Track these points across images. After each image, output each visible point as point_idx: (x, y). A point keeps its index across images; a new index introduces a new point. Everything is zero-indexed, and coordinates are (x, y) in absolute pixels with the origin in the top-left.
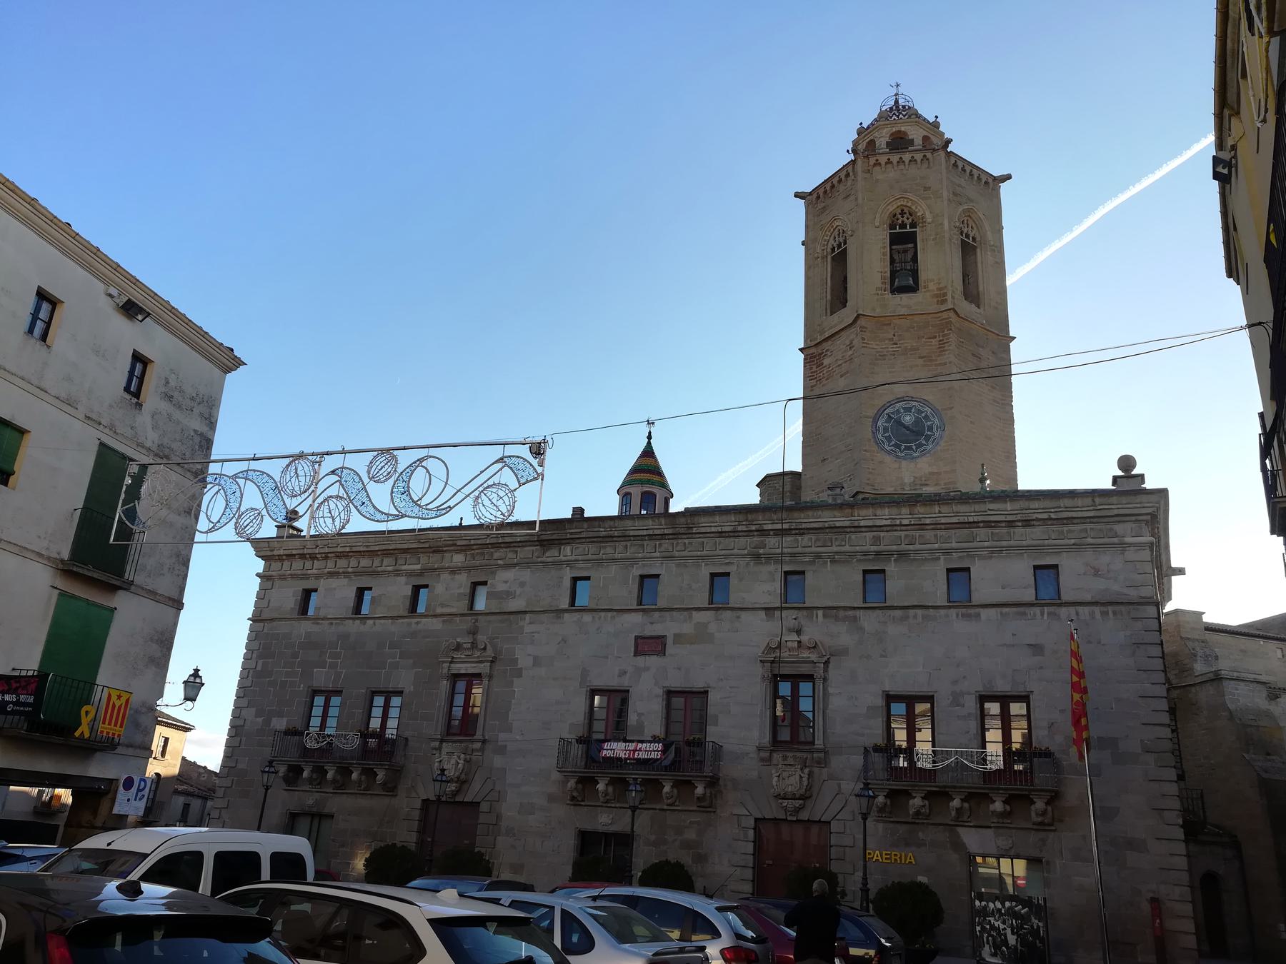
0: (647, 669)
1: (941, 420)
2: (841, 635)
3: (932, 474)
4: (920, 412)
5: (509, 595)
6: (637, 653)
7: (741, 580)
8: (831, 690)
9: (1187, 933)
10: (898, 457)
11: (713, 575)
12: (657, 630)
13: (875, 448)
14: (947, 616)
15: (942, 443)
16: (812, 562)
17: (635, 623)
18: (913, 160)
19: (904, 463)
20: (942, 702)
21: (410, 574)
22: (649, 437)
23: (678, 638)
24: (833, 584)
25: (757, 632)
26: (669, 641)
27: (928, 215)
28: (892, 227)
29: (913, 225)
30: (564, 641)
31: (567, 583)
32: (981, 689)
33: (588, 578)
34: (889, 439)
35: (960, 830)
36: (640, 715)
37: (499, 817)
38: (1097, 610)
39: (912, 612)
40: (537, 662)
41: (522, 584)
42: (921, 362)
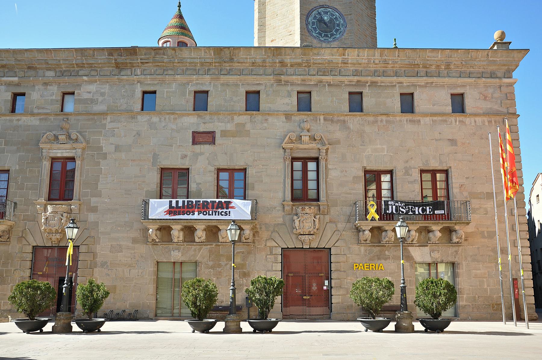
0: (201, 154)
1: (344, 21)
5: (93, 101)
6: (194, 143)
7: (268, 95)
8: (330, 167)
9: (530, 296)
11: (144, 93)
13: (308, 34)
14: (401, 121)
15: (345, 35)
16: (316, 85)
17: (194, 122)
20: (399, 175)
21: (9, 84)
22: (179, 6)
23: (225, 134)
24: (330, 99)
25: (278, 126)
26: (218, 136)
30: (138, 134)
31: (140, 95)
32: (421, 165)
33: (73, 93)
34: (315, 29)
35: (410, 248)
36: (198, 184)
37: (95, 255)
38: (486, 119)
39: (379, 118)
40: (118, 148)
41: (103, 94)
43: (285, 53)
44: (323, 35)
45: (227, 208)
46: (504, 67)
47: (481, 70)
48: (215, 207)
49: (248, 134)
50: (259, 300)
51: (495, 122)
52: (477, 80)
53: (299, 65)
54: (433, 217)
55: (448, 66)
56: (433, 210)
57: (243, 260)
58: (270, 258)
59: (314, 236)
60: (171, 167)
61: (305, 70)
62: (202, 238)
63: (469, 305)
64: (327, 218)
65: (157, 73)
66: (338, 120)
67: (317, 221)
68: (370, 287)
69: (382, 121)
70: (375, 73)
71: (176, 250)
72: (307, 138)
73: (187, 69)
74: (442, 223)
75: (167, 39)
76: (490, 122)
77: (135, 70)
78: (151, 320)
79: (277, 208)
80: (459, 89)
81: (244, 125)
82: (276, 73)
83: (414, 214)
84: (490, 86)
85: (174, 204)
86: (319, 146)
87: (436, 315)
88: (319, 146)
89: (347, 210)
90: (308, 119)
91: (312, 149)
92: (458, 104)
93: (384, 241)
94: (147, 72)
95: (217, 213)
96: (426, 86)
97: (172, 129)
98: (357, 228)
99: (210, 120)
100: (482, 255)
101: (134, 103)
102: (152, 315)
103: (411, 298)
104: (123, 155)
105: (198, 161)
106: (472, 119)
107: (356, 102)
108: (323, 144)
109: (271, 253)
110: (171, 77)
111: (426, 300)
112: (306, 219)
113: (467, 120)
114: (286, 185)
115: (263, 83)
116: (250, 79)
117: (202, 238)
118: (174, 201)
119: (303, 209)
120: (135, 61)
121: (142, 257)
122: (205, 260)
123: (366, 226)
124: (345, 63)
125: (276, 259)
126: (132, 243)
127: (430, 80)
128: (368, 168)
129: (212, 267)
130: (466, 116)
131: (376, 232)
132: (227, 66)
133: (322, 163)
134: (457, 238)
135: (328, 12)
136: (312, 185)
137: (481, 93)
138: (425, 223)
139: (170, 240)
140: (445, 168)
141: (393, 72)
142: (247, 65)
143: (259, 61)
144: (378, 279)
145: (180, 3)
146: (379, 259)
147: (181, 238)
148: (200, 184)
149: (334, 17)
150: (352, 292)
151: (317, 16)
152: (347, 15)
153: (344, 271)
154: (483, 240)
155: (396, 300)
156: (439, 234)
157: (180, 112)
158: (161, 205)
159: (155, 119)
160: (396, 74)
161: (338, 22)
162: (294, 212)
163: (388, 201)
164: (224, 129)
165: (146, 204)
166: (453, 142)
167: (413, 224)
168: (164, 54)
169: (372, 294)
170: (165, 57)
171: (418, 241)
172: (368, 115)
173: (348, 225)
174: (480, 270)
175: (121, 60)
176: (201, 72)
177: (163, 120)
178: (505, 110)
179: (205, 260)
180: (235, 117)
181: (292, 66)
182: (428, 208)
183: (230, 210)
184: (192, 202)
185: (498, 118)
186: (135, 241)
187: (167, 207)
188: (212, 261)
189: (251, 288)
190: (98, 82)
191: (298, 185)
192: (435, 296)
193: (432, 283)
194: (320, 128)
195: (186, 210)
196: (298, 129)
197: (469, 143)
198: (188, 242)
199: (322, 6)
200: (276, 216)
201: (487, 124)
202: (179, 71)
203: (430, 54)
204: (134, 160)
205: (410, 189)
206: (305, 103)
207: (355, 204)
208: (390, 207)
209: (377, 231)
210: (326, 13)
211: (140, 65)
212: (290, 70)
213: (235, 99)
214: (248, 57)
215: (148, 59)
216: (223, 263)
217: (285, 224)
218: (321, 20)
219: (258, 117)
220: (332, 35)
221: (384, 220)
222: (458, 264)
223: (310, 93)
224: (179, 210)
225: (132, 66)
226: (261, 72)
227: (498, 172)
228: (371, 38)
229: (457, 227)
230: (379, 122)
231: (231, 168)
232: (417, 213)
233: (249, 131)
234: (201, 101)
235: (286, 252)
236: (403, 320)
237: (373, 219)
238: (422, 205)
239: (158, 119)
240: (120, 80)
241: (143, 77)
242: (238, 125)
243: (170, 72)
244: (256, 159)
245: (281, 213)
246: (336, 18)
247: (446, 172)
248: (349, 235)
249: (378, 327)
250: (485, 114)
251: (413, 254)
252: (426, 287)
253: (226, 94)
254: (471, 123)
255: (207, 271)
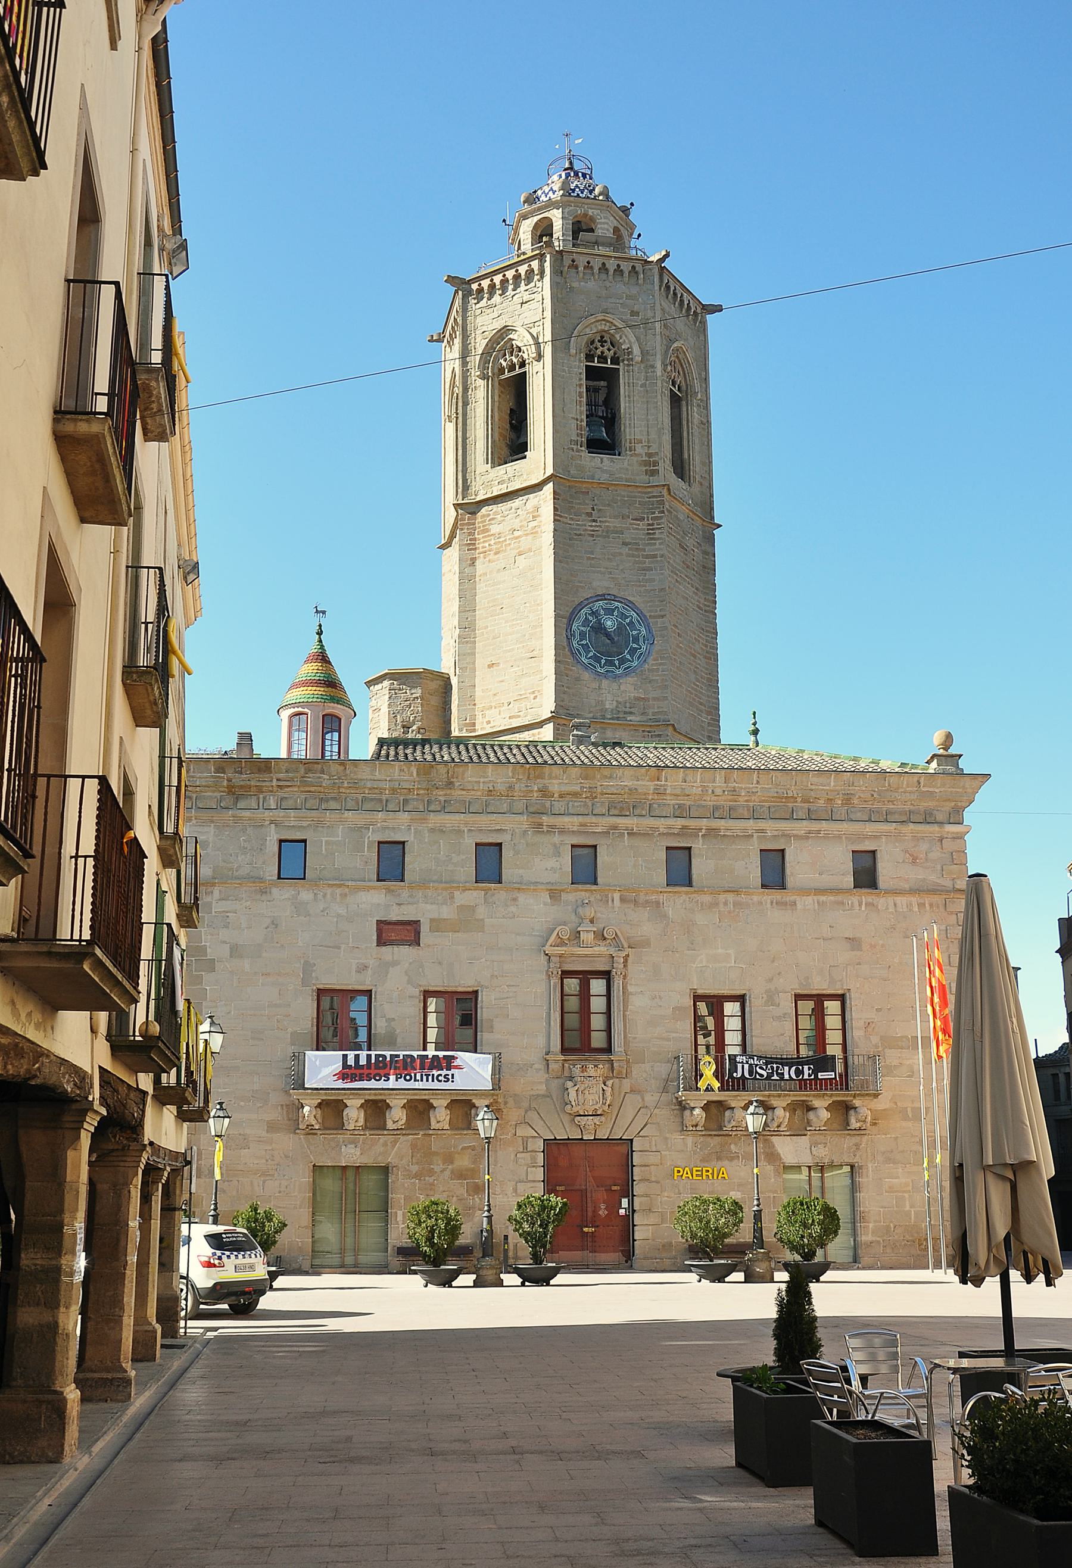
0: (395, 963)
2: (645, 926)
3: (639, 699)
4: (623, 616)
6: (381, 942)
7: (517, 853)
8: (630, 989)
10: (598, 674)
11: (281, 841)
12: (407, 913)
13: (570, 660)
15: (650, 661)
17: (378, 902)
18: (619, 270)
19: (605, 683)
20: (755, 1004)
22: (320, 633)
23: (437, 925)
25: (534, 913)
26: (424, 929)
27: (636, 350)
28: (589, 357)
29: (615, 360)
30: (275, 924)
32: (797, 986)
35: (774, 1139)
38: (914, 900)
39: (722, 897)
40: (236, 951)
42: (625, 550)
43: (550, 774)
44: (603, 661)
45: (449, 1069)
46: (948, 803)
47: (907, 807)
48: (427, 1066)
49: (480, 926)
50: (529, 1233)
51: (931, 905)
52: (899, 826)
53: (575, 794)
54: (816, 1084)
55: (848, 800)
56: (815, 1072)
57: (474, 1162)
58: (524, 1158)
59: (603, 1118)
60: (338, 987)
61: (586, 805)
62: (401, 1123)
63: (879, 1242)
64: (627, 1084)
65: (308, 806)
66: (647, 902)
67: (608, 1090)
68: (706, 1211)
69: (726, 904)
70: (715, 812)
71: (350, 1143)
72: (591, 936)
73: (364, 799)
74: (831, 1096)
75: (300, 709)
76: (921, 905)
77: (264, 798)
78: (307, 1273)
79: (536, 1066)
80: (867, 843)
81: (472, 909)
82: (531, 810)
83: (782, 1079)
84: (923, 838)
85: (351, 1061)
86: (612, 951)
87: (809, 1255)
88: (612, 951)
89: (663, 1069)
90: (592, 899)
91: (600, 956)
92: (866, 875)
93: (729, 1127)
94: (290, 803)
95: (430, 1078)
96: (808, 838)
97: (339, 916)
98: (680, 1103)
99: (410, 900)
100: (903, 1152)
101: (264, 863)
102: (306, 1266)
103: (770, 1228)
104: (246, 965)
105: (389, 976)
106: (890, 900)
107: (680, 869)
108: (620, 948)
109: (525, 1150)
110: (335, 816)
111: (793, 1232)
112: (590, 1088)
113: (882, 902)
114: (552, 1023)
115: (509, 828)
116: (484, 820)
117: (401, 1123)
118: (351, 1055)
119: (584, 1069)
120: (267, 784)
121: (286, 1157)
122: (404, 1161)
123: (697, 1101)
124: (660, 792)
125: (534, 1159)
126: (268, 1132)
127: (815, 826)
128: (700, 992)
129: (417, 1176)
130: (878, 895)
131: (714, 1110)
132: (440, 795)
133: (617, 983)
134: (858, 1121)
135: (613, 610)
136: (597, 1022)
137: (906, 852)
138: (800, 1095)
139: (340, 1126)
140: (840, 992)
141: (748, 810)
142: (479, 793)
143: (501, 787)
144: (718, 1200)
145: (320, 626)
146: (719, 1159)
147: (361, 1122)
148: (393, 1019)
149: (628, 621)
150: (678, 1219)
151: (590, 618)
152: (654, 617)
153: (658, 1182)
154: (904, 1124)
155: (745, 1234)
156: (825, 1115)
157: (354, 883)
158: (327, 1063)
159: (306, 895)
160: (754, 815)
161: (634, 632)
162: (566, 1074)
163: (735, 1056)
164: (435, 916)
165: (298, 1059)
166: (854, 942)
167: (779, 1096)
168: (322, 772)
169: (708, 1222)
170: (325, 776)
171: (790, 1127)
172: (700, 891)
173: (665, 1098)
174: (897, 1177)
175: (238, 780)
176: (391, 807)
177: (320, 896)
178: (948, 884)
179: (404, 1161)
180: (457, 893)
181: (561, 796)
182: (806, 1067)
183: (453, 1071)
184: (384, 1057)
185: (938, 899)
186: (272, 1127)
187: (338, 1066)
188: (417, 1163)
189: (515, 1213)
190: (194, 821)
191: (573, 1021)
192: (805, 1226)
193: (802, 1204)
194: (614, 915)
195: (373, 1071)
196: (573, 917)
197: (883, 945)
198: (373, 1129)
199: (602, 597)
200: (533, 1081)
201: (916, 909)
202: (351, 804)
203: (815, 780)
204: (269, 974)
205: (777, 1032)
206: (585, 868)
207: (677, 1058)
208: (740, 1066)
209: (716, 1109)
210: (610, 612)
211: (275, 789)
212: (559, 807)
213: (455, 859)
214: (482, 780)
215: (292, 779)
216: (437, 1169)
217: (550, 1097)
218: (599, 629)
219: (500, 894)
220: (623, 661)
221: (728, 1090)
222: (861, 1167)
223: (595, 847)
224: (361, 1071)
225: (260, 789)
226: (505, 807)
227: (924, 1012)
228: (705, 657)
229: (857, 1102)
230: (721, 905)
231: (449, 989)
232: (786, 1077)
233: (482, 920)
234: (391, 861)
235: (552, 1147)
236: (756, 1263)
237: (709, 1089)
238: (797, 1062)
239: (311, 896)
240: (237, 819)
241: (282, 813)
242: (461, 908)
243: (333, 805)
244: (496, 973)
245: (542, 1076)
246: (631, 623)
247: (842, 998)
248: (665, 1115)
249: (718, 1275)
250: (912, 891)
251: (780, 1151)
252: (793, 1212)
253: (439, 849)
254: (887, 908)
255: (407, 1183)
